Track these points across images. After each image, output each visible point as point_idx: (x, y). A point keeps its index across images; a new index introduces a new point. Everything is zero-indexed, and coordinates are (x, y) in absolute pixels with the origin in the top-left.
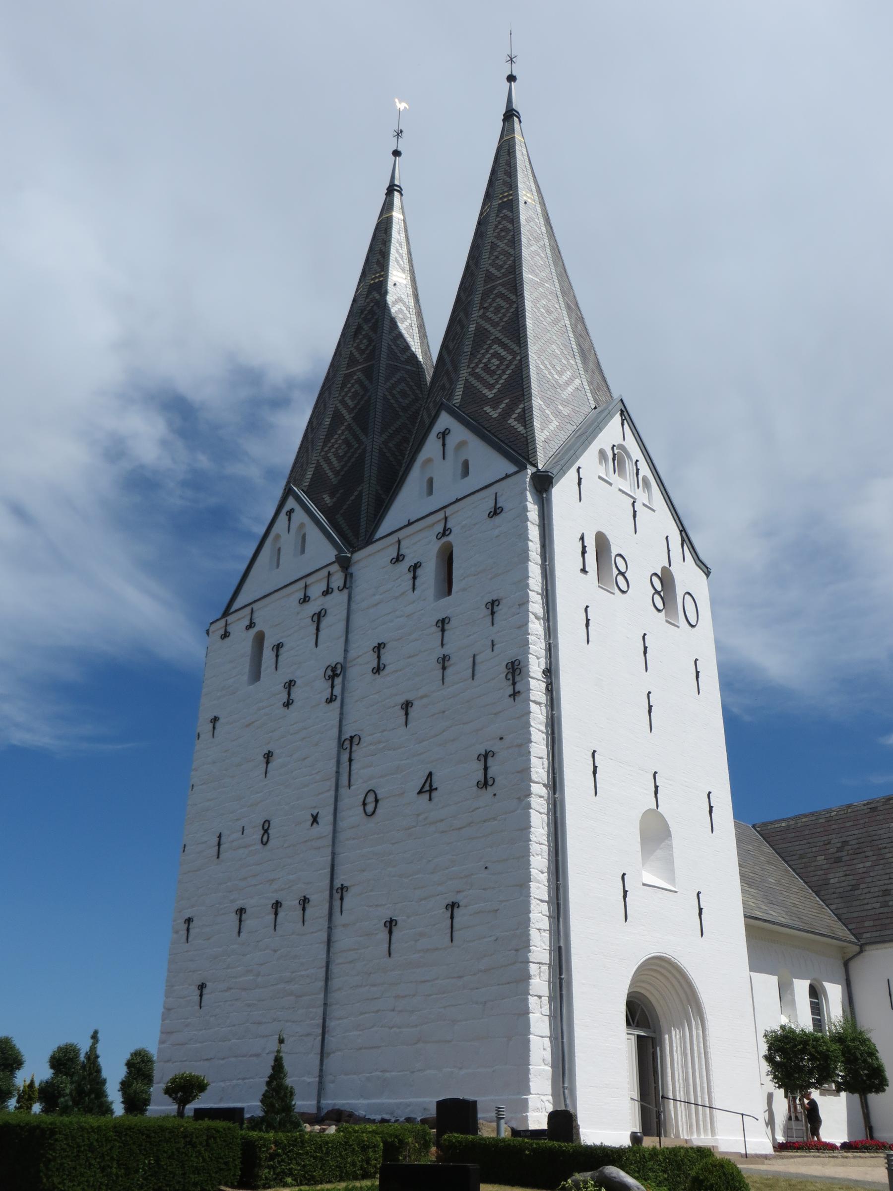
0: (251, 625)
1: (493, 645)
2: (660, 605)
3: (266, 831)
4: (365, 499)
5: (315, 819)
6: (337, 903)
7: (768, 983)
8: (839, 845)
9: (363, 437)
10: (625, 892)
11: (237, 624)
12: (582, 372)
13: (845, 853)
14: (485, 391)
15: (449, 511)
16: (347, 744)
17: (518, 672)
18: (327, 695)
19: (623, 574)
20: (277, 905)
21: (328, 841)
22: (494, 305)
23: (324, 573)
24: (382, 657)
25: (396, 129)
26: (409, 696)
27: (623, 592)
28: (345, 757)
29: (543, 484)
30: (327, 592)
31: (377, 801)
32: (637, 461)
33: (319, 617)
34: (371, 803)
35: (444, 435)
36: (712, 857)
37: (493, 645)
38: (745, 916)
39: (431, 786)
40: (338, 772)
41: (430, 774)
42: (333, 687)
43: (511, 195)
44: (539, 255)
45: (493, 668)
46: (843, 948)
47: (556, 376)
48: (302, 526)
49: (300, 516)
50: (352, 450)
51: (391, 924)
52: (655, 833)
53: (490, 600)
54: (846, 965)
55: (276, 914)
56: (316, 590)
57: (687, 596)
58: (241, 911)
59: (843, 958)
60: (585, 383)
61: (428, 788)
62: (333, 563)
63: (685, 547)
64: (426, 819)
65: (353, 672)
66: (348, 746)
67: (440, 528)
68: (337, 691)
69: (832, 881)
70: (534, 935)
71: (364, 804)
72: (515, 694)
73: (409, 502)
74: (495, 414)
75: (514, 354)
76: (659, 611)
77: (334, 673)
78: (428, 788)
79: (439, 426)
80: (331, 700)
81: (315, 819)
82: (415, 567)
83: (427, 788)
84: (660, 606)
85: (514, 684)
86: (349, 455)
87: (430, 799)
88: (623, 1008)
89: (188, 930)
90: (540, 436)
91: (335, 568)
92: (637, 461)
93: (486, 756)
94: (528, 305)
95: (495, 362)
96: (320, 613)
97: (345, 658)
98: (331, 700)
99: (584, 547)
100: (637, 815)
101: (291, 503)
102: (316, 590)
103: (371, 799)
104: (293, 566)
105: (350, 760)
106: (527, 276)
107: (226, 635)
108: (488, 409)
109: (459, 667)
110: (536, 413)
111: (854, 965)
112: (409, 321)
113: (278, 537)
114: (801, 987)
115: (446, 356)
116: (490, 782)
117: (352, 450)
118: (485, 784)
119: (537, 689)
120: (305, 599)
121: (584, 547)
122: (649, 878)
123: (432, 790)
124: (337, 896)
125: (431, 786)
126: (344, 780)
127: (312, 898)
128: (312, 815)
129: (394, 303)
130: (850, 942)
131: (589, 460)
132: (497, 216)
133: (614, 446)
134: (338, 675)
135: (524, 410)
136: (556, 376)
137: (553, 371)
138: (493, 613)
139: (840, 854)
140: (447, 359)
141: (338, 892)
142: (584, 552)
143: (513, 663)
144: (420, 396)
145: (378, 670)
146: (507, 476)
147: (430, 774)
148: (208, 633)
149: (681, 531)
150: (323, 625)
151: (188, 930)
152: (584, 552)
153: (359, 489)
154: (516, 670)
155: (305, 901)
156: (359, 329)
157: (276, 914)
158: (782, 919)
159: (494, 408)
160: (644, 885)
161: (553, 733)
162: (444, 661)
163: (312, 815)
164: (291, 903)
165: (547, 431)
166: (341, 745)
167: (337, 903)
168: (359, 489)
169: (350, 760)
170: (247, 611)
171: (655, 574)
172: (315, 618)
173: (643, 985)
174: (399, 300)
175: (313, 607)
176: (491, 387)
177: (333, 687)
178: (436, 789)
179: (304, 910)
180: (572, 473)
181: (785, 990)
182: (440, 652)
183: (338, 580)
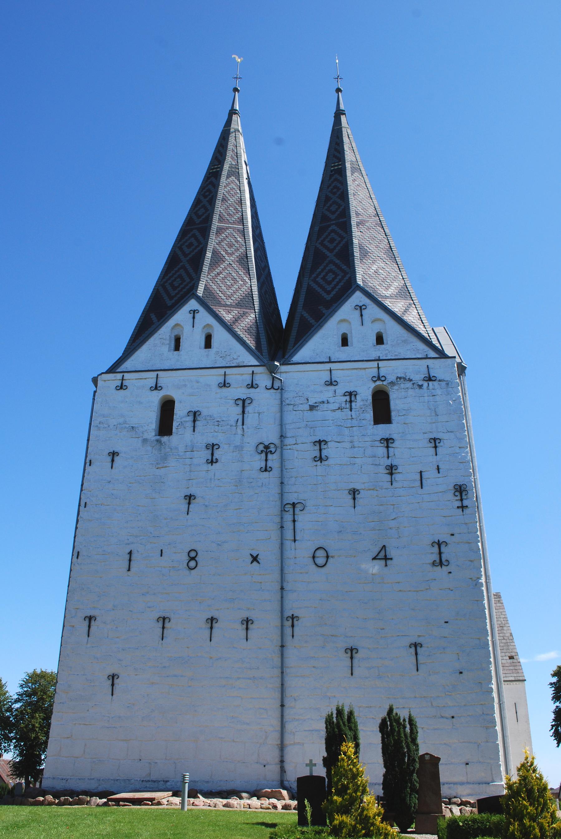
6: (288, 631)
16: (290, 508)
17: (464, 493)
22: (330, 237)
33: (244, 403)
43: (340, 165)
45: (440, 486)
67: (374, 372)
85: (462, 500)
86: (182, 286)
124: (288, 623)
126: (289, 535)
156: (327, 199)
162: (391, 470)
166: (283, 510)
167: (288, 631)
176: (329, 293)
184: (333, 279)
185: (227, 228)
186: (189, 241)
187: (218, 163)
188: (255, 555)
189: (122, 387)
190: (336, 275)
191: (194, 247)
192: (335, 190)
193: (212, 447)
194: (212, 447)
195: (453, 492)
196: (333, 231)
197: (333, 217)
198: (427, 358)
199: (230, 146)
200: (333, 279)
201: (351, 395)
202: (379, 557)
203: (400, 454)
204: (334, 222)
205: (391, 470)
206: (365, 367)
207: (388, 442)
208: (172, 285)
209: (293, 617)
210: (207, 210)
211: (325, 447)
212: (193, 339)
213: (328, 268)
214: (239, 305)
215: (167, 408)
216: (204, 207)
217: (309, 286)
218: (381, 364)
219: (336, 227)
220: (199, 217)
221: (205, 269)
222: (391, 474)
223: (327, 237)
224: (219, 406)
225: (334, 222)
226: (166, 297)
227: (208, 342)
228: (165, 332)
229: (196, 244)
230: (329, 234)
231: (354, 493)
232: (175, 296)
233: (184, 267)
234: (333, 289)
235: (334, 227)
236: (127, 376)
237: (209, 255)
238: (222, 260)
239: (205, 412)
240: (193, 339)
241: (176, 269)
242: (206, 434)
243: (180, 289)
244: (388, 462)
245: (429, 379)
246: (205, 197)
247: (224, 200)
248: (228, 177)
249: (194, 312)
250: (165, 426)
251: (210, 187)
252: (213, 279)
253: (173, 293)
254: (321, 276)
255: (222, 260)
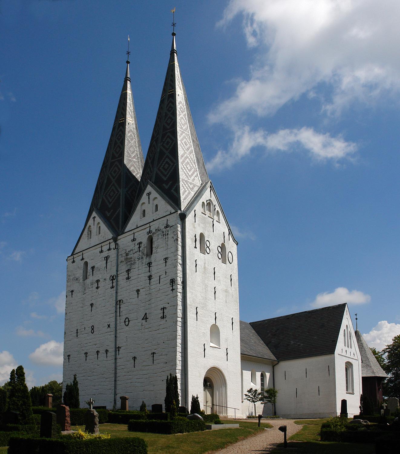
0: (83, 259)
1: (166, 273)
2: (220, 257)
3: (93, 329)
4: (121, 214)
5: (109, 326)
7: (247, 374)
8: (276, 330)
9: (119, 189)
10: (205, 349)
11: (78, 259)
12: (197, 169)
13: (277, 333)
14: (163, 177)
15: (151, 224)
16: (119, 303)
18: (111, 285)
19: (208, 247)
20: (98, 352)
21: (114, 333)
23: (108, 242)
24: (129, 274)
25: (127, 51)
26: (139, 288)
27: (208, 254)
28: (118, 306)
29: (183, 217)
30: (109, 249)
31: (129, 321)
32: (215, 205)
33: (107, 258)
34: (127, 321)
35: (149, 194)
36: (232, 338)
37: (166, 273)
38: (241, 354)
39: (146, 317)
40: (116, 312)
41: (146, 313)
42: (113, 283)
43: (123, 120)
44: (183, 119)
46: (273, 362)
47: (188, 172)
48: (99, 223)
49: (98, 219)
50: (115, 194)
51: (135, 358)
52: (215, 331)
53: (165, 258)
54: (273, 367)
55: (98, 355)
56: (105, 248)
57: (229, 253)
58: (86, 353)
59: (272, 365)
60: (198, 174)
61: (145, 318)
62: (111, 239)
63: (230, 235)
64: (145, 327)
65: (120, 278)
66: (119, 303)
67: (148, 230)
68: (114, 284)
69: (272, 342)
70: (178, 361)
71: (125, 322)
72: (173, 290)
73: (135, 219)
74: (167, 187)
75: (172, 162)
76: (220, 259)
77: (113, 278)
78: (145, 318)
79: (147, 191)
80: (112, 287)
81: (109, 326)
82: (140, 243)
83: (145, 318)
84: (220, 257)
85: (172, 286)
87: (146, 321)
88: (203, 381)
89: (69, 359)
90: (182, 197)
91: (112, 241)
92: (215, 205)
93: (163, 309)
94: (179, 142)
95: (167, 165)
96: (107, 257)
97: (117, 273)
98: (112, 287)
99: (196, 239)
100: (209, 326)
101: (94, 214)
102: (105, 248)
103: (127, 320)
104: (95, 240)
105: (120, 308)
106: (180, 152)
107: (74, 262)
108: (164, 185)
109: (155, 279)
110: (181, 187)
111: (276, 367)
112: (134, 140)
113: (90, 226)
114: (258, 374)
115: (149, 159)
116: (165, 317)
117: (115, 194)
118: (163, 317)
119: (180, 288)
120: (102, 251)
121: (196, 239)
122: (212, 345)
123: (146, 318)
125: (146, 317)
126: (118, 314)
127: (110, 350)
128: (108, 325)
129: (129, 132)
130: (275, 360)
131: (198, 207)
132: (168, 101)
133: (207, 200)
134: (114, 279)
135: (177, 187)
136: (188, 172)
137: (187, 170)
138: (166, 262)
139: (276, 333)
140: (150, 161)
141: (117, 349)
142: (196, 241)
143: (172, 279)
144: (139, 172)
145: (128, 278)
146: (171, 214)
147: (146, 313)
148: (67, 261)
149: (229, 230)
150: (108, 261)
151: (69, 359)
152: (196, 241)
153: (118, 210)
154: (173, 282)
155: (107, 351)
157: (98, 355)
158: (254, 354)
159: (167, 185)
160: (210, 347)
161: (184, 315)
162: (150, 277)
163: (108, 325)
164: (102, 351)
165: (186, 195)
166: (117, 304)
168: (118, 210)
169: (120, 308)
170: (81, 253)
171: (219, 246)
172: (106, 258)
173: (210, 375)
174: (130, 131)
175: (105, 254)
176: (165, 176)
177: (113, 283)
178: (148, 318)
179: (107, 354)
180: (193, 212)
181: (253, 376)
182: (149, 274)
183: (113, 245)
187: (122, 117)
194: (98, 281)
195: (170, 283)
200: (168, 167)
202: (144, 318)
206: (145, 228)
209: (119, 347)
210: (120, 148)
211: (130, 272)
222: (150, 279)
225: (169, 130)
229: (171, 142)
232: (167, 174)
233: (167, 157)
243: (169, 170)
251: (120, 133)
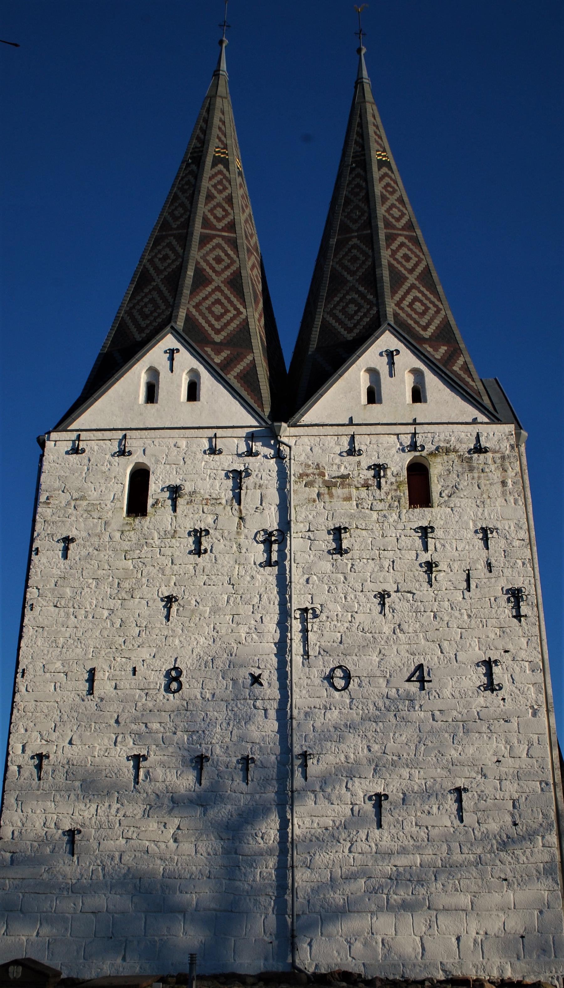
33: (238, 477)
162: (430, 567)
176: (350, 330)
184: (356, 312)
185: (214, 236)
186: (164, 253)
188: (256, 675)
189: (76, 450)
190: (360, 307)
191: (169, 261)
192: (357, 190)
193: (198, 535)
196: (355, 246)
197: (355, 227)
198: (475, 421)
199: (216, 121)
201: (379, 470)
202: (412, 679)
203: (443, 550)
204: (356, 234)
205: (430, 567)
207: (425, 532)
208: (141, 312)
212: (175, 385)
213: (348, 297)
214: (228, 343)
215: (140, 478)
216: (182, 205)
217: (333, 268)
218: (419, 429)
219: (359, 242)
220: (176, 219)
221: (186, 292)
223: (347, 254)
224: (208, 478)
226: (133, 329)
227: (193, 393)
228: (136, 377)
230: (350, 250)
231: (383, 596)
234: (355, 326)
235: (355, 241)
236: (84, 435)
237: (190, 273)
238: (209, 281)
239: (188, 487)
240: (175, 385)
241: (146, 290)
242: (189, 517)
244: (425, 557)
245: (479, 449)
246: (183, 191)
247: (210, 197)
248: (214, 165)
249: (172, 353)
250: (138, 504)
252: (197, 306)
253: (143, 324)
254: (339, 308)
255: (209, 281)
